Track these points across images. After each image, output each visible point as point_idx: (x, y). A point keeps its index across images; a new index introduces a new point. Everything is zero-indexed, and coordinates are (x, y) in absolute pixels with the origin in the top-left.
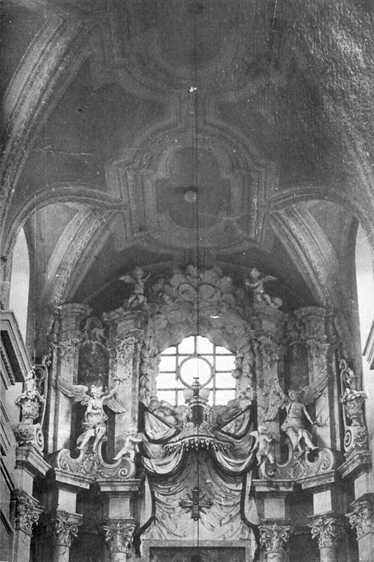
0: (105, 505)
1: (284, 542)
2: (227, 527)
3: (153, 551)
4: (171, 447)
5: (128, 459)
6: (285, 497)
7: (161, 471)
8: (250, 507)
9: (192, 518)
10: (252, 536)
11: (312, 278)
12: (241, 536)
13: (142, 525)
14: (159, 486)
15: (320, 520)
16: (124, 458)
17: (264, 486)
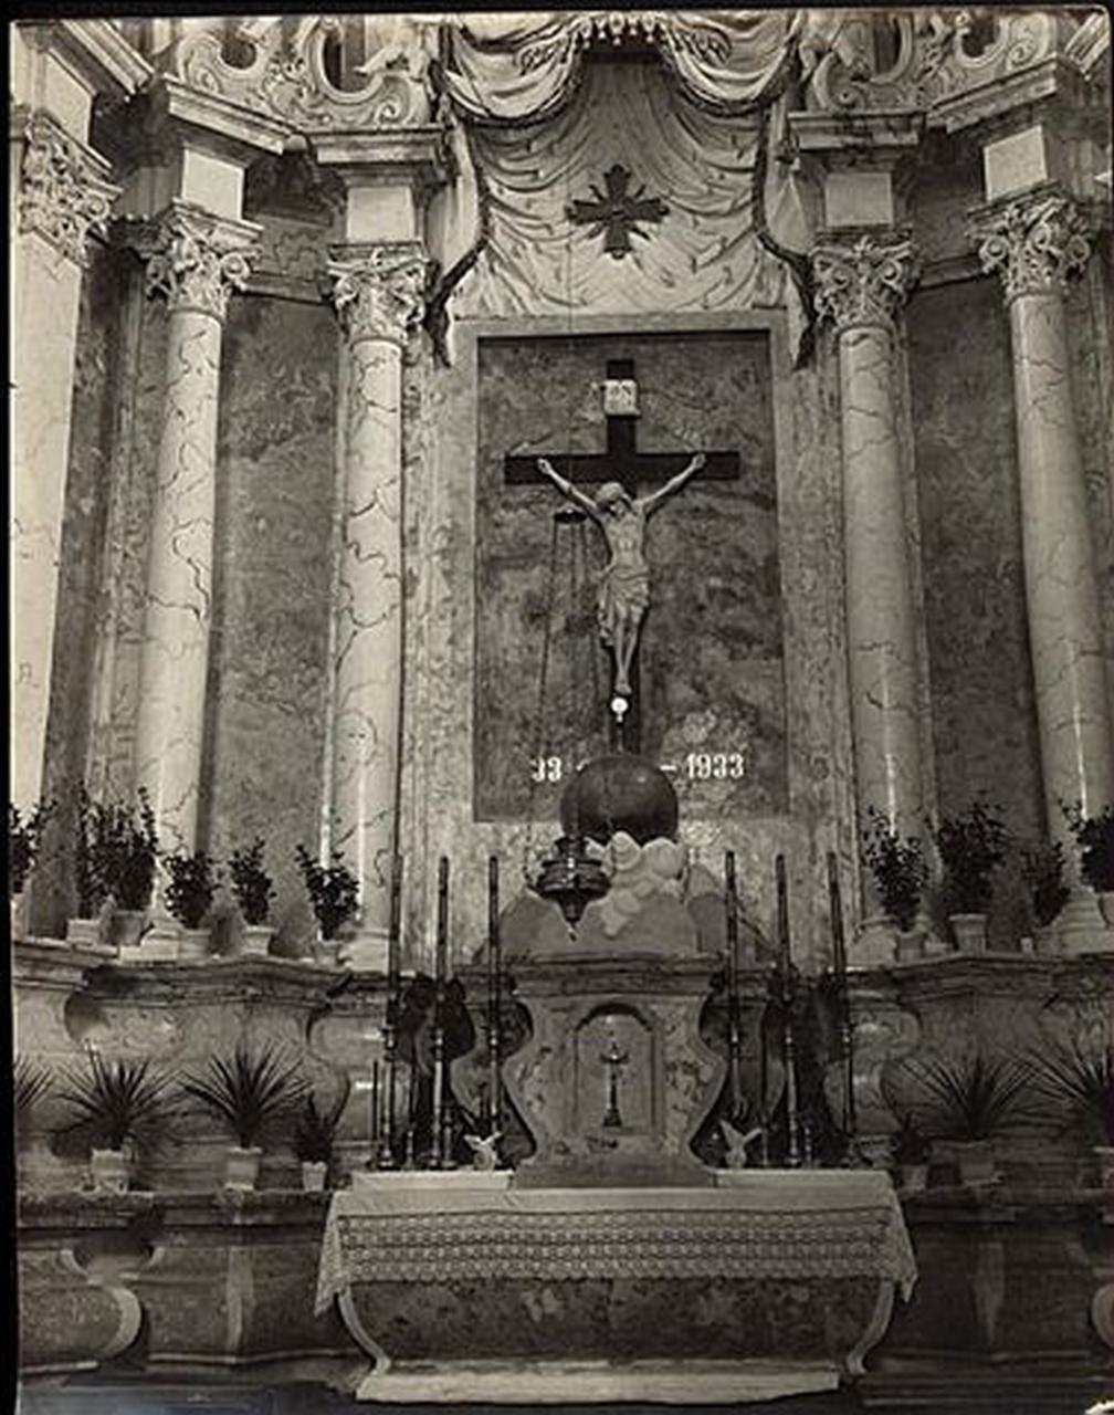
0: (338, 218)
1: (893, 292)
2: (716, 271)
3: (488, 352)
4: (538, 52)
5: (404, 74)
6: (891, 166)
7: (513, 108)
8: (785, 201)
9: (607, 250)
10: (791, 293)
11: (792, 331)
12: (760, 297)
13: (446, 271)
14: (503, 163)
15: (1011, 211)
16: (391, 73)
17: (824, 131)
